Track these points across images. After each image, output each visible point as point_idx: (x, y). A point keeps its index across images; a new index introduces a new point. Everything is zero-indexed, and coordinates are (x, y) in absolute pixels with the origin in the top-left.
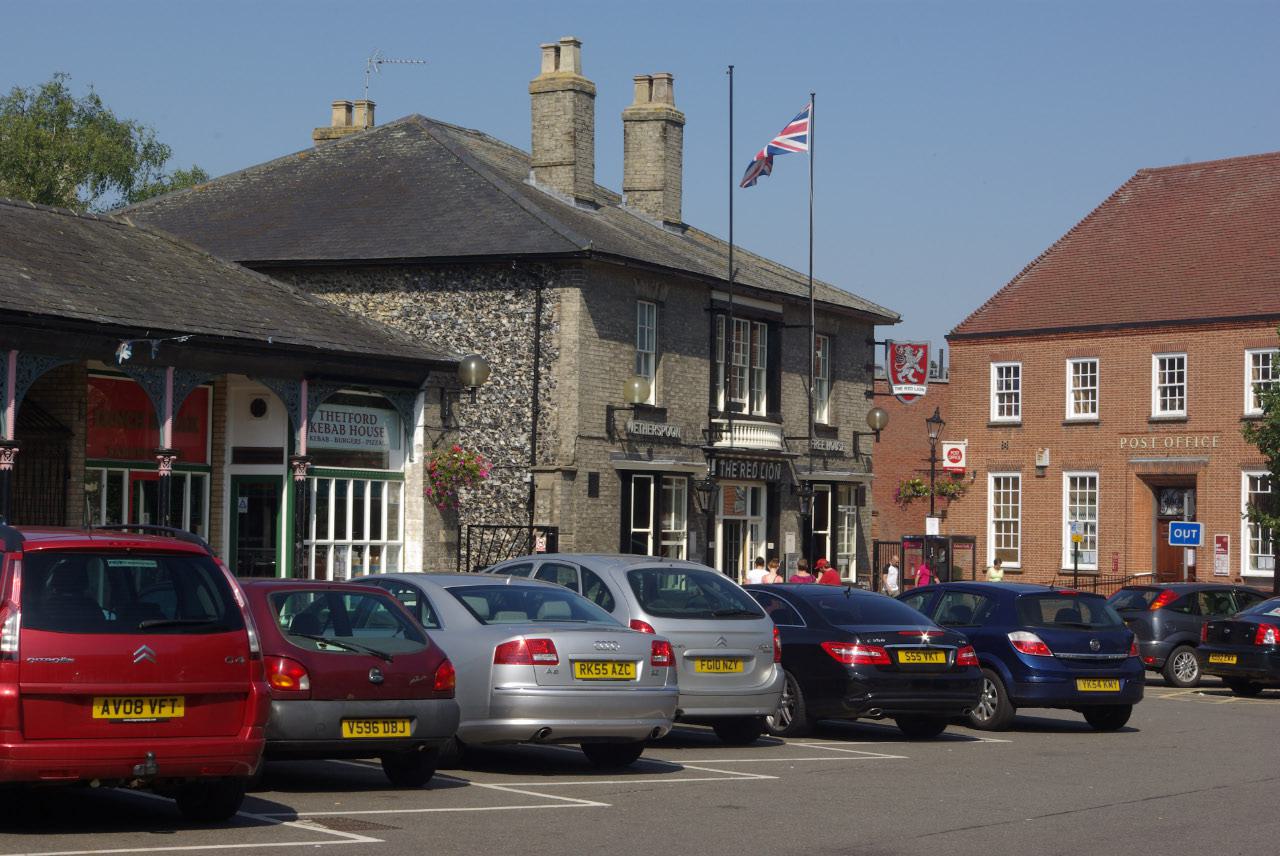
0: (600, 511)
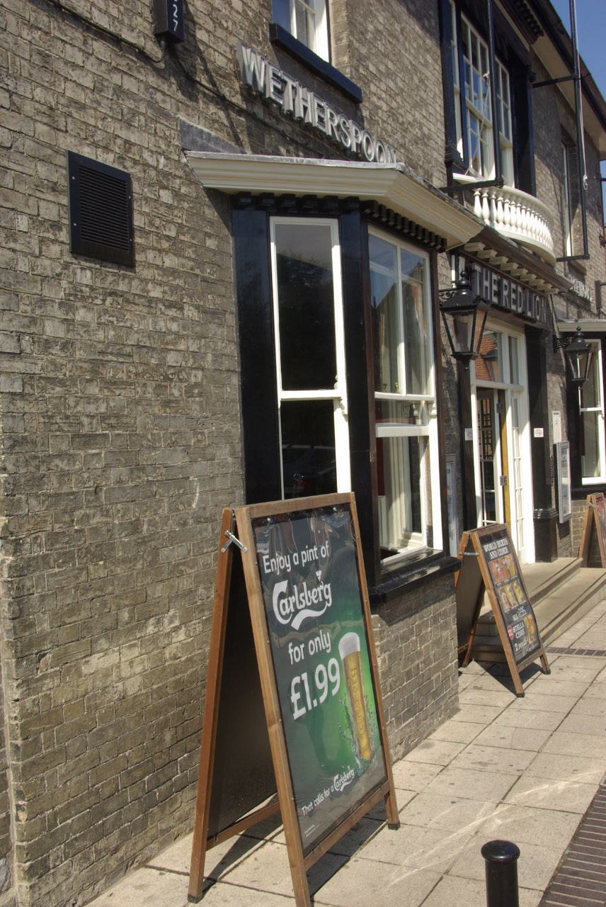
0: (140, 324)
